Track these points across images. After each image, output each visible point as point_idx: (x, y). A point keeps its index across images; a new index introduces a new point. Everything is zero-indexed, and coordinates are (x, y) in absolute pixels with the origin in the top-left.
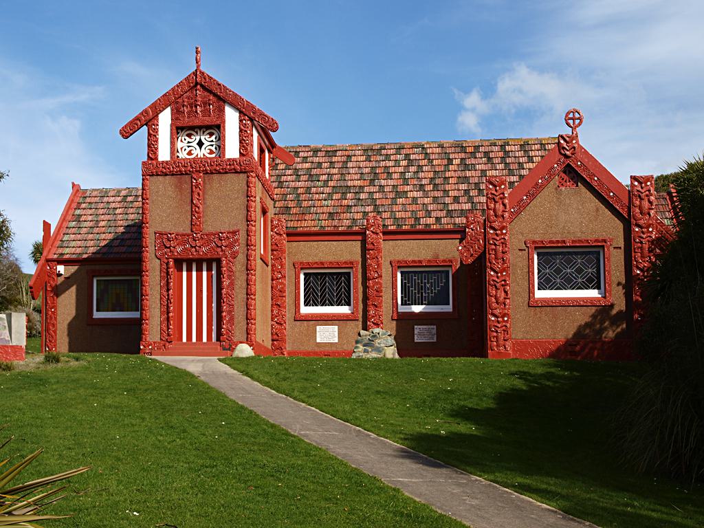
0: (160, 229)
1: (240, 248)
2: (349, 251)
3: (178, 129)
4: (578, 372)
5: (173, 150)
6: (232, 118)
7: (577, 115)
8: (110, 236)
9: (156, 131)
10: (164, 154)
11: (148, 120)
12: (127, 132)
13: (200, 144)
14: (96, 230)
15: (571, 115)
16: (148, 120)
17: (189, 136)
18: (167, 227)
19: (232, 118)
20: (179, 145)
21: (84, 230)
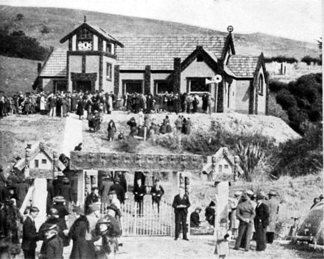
0: (73, 72)
1: (98, 78)
2: (140, 77)
3: (78, 41)
4: (78, 107)
5: (77, 47)
6: (96, 38)
7: (231, 28)
8: (192, 51)
9: (72, 41)
10: (74, 49)
11: (69, 37)
12: (63, 41)
13: (86, 45)
14: (140, 51)
15: (230, 28)
16: (69, 37)
17: (82, 42)
18: (75, 72)
19: (96, 38)
20: (79, 45)
21: (136, 51)
